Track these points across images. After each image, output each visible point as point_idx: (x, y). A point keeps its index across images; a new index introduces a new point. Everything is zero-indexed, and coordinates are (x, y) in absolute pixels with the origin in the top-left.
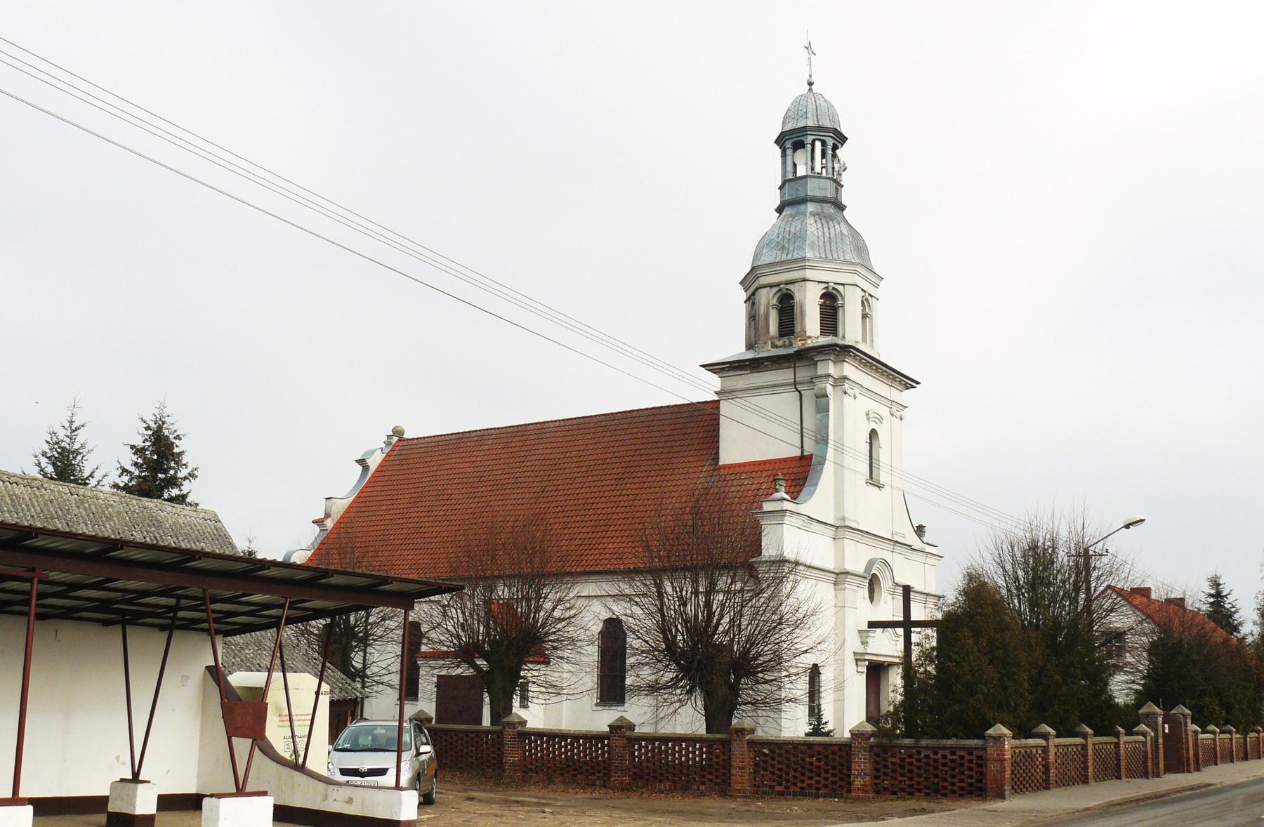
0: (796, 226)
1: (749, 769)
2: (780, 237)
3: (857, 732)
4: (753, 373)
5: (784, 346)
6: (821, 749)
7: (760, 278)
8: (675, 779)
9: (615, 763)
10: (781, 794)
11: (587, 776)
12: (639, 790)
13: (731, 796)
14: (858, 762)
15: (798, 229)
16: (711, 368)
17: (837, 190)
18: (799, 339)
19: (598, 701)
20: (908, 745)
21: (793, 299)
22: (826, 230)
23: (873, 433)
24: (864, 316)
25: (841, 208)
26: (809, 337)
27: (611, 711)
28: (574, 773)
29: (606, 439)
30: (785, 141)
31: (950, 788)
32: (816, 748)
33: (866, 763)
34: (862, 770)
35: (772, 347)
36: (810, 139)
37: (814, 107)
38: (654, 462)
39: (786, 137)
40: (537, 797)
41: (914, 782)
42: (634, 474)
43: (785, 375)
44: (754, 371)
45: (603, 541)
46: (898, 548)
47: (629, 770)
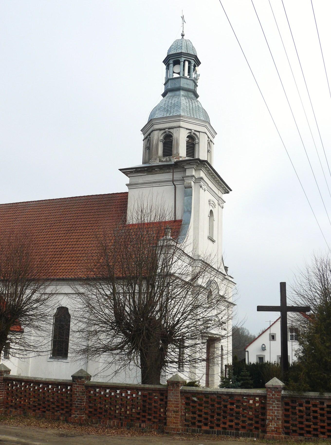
0: (175, 100)
1: (181, 412)
2: (166, 105)
3: (271, 387)
4: (148, 175)
5: (166, 161)
6: (239, 398)
7: (154, 125)
8: (121, 417)
9: (76, 404)
10: (207, 432)
11: (53, 413)
12: (93, 425)
13: (167, 433)
14: (272, 410)
15: (176, 102)
16: (125, 171)
17: (195, 88)
18: (175, 157)
19: (51, 355)
20: (313, 397)
21: (172, 137)
22: (191, 104)
23: (211, 212)
24: (208, 151)
25: (197, 96)
26: (181, 157)
27: (58, 362)
28: (43, 410)
29: (61, 210)
30: (170, 59)
31: (313, 426)
32: (237, 398)
33: (278, 410)
34: (275, 416)
35: (160, 162)
36: (183, 59)
37: (186, 44)
38: (88, 222)
39: (170, 58)
40: (17, 435)
41: (318, 427)
42: (77, 228)
43: (167, 176)
44: (148, 173)
45: (61, 260)
46: (220, 276)
47: (86, 410)
